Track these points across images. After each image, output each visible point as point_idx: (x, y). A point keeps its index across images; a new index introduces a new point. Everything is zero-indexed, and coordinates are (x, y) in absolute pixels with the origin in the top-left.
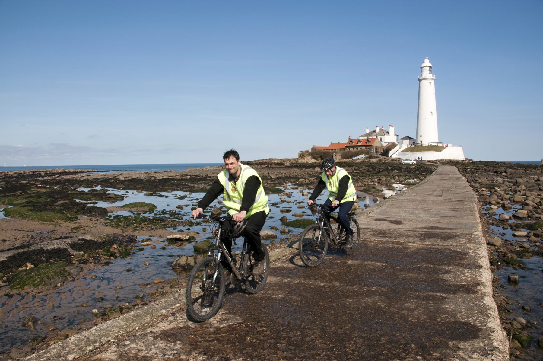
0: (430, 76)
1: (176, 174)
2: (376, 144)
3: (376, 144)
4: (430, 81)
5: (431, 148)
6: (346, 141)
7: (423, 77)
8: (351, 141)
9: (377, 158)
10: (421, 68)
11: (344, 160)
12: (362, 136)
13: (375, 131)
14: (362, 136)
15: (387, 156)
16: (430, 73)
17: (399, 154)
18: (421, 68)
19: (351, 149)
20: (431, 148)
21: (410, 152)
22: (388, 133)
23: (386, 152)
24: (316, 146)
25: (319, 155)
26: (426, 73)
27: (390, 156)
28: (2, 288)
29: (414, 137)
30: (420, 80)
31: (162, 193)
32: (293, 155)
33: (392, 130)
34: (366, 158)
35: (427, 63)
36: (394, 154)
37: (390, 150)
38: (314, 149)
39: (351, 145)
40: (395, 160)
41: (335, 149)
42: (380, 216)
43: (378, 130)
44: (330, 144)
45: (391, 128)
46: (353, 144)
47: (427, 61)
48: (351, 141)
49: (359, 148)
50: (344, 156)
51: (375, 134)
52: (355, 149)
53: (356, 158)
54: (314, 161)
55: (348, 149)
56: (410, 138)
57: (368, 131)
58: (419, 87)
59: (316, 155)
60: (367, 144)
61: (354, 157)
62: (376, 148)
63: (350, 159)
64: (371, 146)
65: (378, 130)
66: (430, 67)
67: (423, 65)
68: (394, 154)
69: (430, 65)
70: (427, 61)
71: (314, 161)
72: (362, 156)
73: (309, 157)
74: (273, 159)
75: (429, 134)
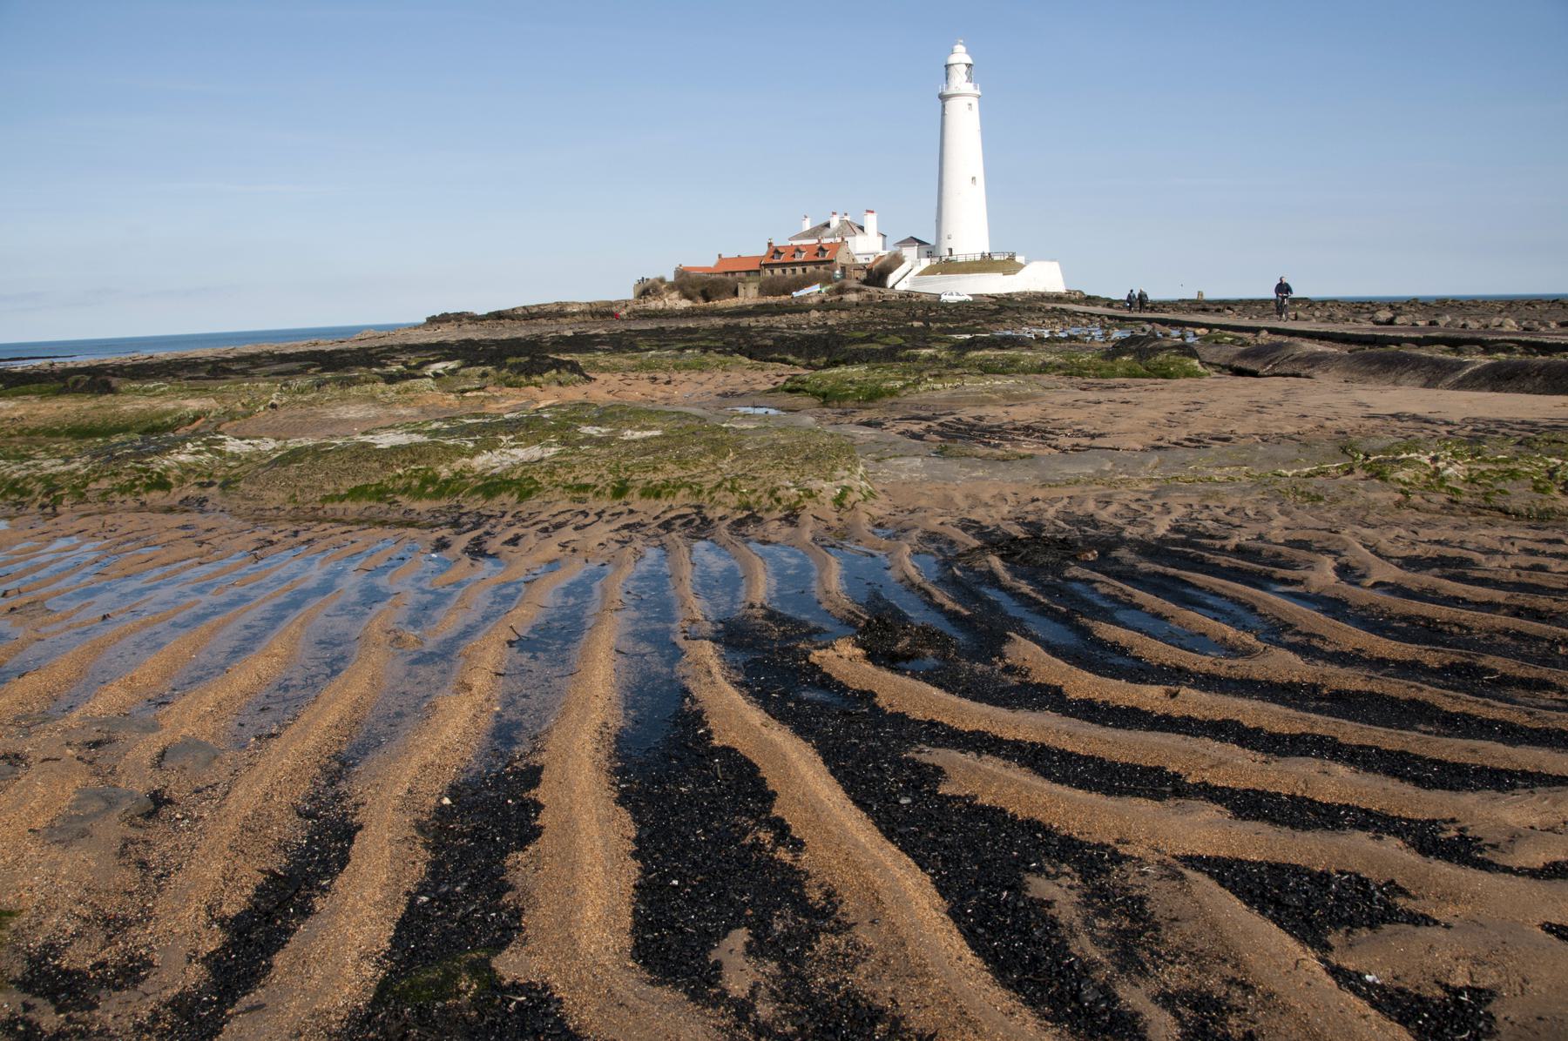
0: (969, 88)
1: (163, 354)
2: (841, 258)
3: (841, 258)
5: (985, 264)
6: (761, 251)
8: (777, 252)
9: (858, 291)
10: (947, 67)
11: (770, 299)
12: (797, 237)
13: (828, 225)
14: (797, 237)
15: (884, 286)
16: (969, 80)
17: (914, 282)
18: (947, 67)
19: (778, 271)
20: (985, 264)
21: (938, 276)
22: (862, 228)
23: (877, 275)
24: (686, 264)
25: (698, 290)
26: (959, 81)
27: (890, 283)
28: (1561, 927)
29: (932, 242)
30: (944, 98)
32: (619, 290)
33: (871, 222)
34: (829, 292)
35: (960, 56)
36: (901, 281)
37: (891, 271)
38: (681, 273)
39: (776, 261)
40: (909, 294)
41: (733, 273)
45: (870, 216)
46: (782, 259)
47: (960, 49)
48: (777, 251)
49: (799, 270)
50: (765, 289)
51: (828, 231)
52: (789, 271)
53: (802, 293)
54: (685, 304)
55: (768, 272)
56: (921, 243)
57: (807, 226)
58: (943, 114)
60: (820, 258)
61: (798, 289)
62: (843, 269)
63: (784, 298)
64: (831, 262)
65: (835, 222)
66: (969, 66)
67: (952, 60)
68: (901, 281)
70: (960, 49)
71: (685, 304)
72: (816, 288)
73: (675, 295)
74: (567, 304)
75: (969, 235)
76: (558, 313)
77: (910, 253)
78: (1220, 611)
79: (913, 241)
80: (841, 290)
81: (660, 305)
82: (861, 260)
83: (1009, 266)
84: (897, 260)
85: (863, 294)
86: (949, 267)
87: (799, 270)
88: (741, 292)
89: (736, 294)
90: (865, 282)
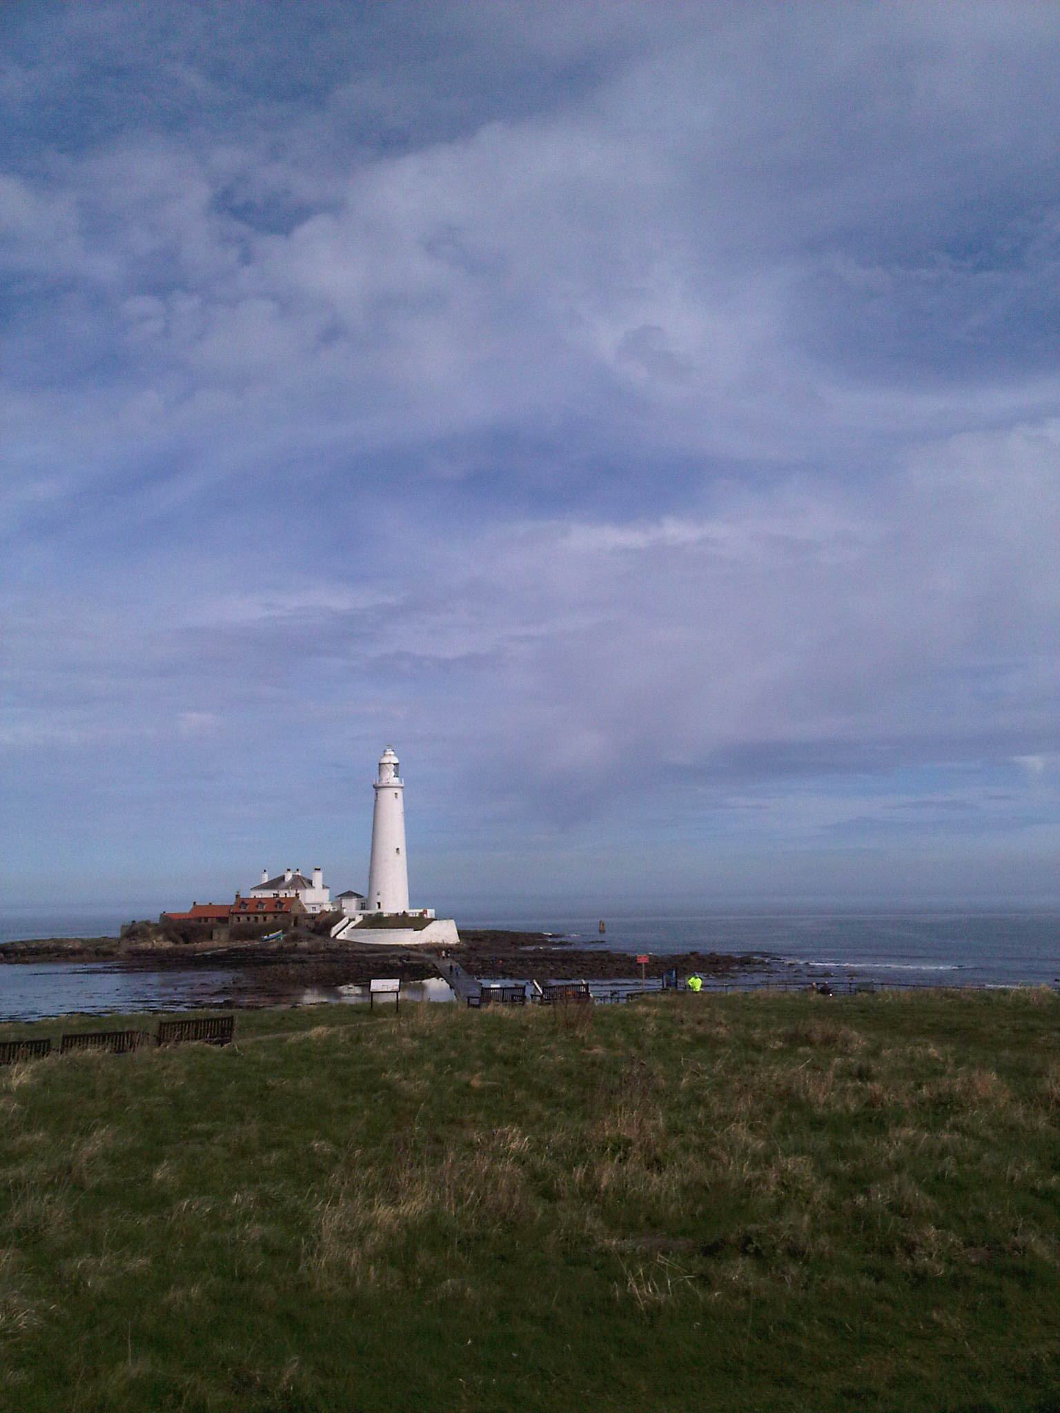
0: (395, 781)
4: (397, 791)
5: (401, 921)
7: (384, 782)
9: (309, 939)
10: (377, 788)
13: (283, 878)
17: (350, 934)
19: (243, 918)
20: (401, 921)
22: (310, 882)
26: (390, 777)
30: (377, 788)
31: (105, 993)
33: (318, 878)
36: (342, 933)
39: (242, 910)
40: (345, 943)
41: (206, 919)
42: (470, 923)
43: (289, 877)
44: (192, 906)
57: (266, 878)
59: (173, 934)
65: (289, 877)
68: (342, 933)
69: (396, 761)
71: (168, 945)
76: (537, 938)
77: (345, 903)
78: (370, 952)
79: (349, 894)
80: (295, 938)
81: (149, 946)
82: (310, 911)
83: (419, 923)
84: (338, 916)
85: (313, 942)
86: (376, 922)
87: (243, 918)
88: (215, 936)
89: (211, 938)
90: (314, 931)
